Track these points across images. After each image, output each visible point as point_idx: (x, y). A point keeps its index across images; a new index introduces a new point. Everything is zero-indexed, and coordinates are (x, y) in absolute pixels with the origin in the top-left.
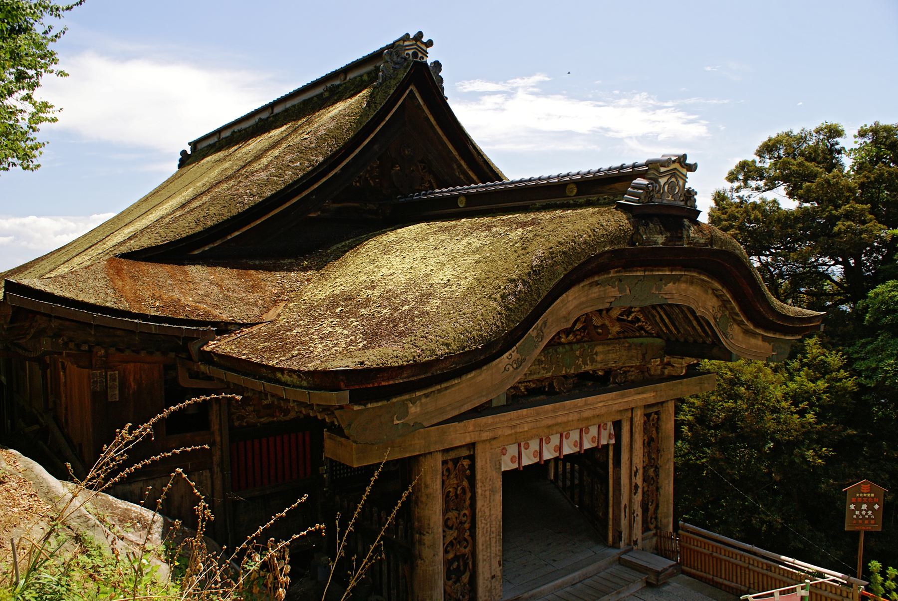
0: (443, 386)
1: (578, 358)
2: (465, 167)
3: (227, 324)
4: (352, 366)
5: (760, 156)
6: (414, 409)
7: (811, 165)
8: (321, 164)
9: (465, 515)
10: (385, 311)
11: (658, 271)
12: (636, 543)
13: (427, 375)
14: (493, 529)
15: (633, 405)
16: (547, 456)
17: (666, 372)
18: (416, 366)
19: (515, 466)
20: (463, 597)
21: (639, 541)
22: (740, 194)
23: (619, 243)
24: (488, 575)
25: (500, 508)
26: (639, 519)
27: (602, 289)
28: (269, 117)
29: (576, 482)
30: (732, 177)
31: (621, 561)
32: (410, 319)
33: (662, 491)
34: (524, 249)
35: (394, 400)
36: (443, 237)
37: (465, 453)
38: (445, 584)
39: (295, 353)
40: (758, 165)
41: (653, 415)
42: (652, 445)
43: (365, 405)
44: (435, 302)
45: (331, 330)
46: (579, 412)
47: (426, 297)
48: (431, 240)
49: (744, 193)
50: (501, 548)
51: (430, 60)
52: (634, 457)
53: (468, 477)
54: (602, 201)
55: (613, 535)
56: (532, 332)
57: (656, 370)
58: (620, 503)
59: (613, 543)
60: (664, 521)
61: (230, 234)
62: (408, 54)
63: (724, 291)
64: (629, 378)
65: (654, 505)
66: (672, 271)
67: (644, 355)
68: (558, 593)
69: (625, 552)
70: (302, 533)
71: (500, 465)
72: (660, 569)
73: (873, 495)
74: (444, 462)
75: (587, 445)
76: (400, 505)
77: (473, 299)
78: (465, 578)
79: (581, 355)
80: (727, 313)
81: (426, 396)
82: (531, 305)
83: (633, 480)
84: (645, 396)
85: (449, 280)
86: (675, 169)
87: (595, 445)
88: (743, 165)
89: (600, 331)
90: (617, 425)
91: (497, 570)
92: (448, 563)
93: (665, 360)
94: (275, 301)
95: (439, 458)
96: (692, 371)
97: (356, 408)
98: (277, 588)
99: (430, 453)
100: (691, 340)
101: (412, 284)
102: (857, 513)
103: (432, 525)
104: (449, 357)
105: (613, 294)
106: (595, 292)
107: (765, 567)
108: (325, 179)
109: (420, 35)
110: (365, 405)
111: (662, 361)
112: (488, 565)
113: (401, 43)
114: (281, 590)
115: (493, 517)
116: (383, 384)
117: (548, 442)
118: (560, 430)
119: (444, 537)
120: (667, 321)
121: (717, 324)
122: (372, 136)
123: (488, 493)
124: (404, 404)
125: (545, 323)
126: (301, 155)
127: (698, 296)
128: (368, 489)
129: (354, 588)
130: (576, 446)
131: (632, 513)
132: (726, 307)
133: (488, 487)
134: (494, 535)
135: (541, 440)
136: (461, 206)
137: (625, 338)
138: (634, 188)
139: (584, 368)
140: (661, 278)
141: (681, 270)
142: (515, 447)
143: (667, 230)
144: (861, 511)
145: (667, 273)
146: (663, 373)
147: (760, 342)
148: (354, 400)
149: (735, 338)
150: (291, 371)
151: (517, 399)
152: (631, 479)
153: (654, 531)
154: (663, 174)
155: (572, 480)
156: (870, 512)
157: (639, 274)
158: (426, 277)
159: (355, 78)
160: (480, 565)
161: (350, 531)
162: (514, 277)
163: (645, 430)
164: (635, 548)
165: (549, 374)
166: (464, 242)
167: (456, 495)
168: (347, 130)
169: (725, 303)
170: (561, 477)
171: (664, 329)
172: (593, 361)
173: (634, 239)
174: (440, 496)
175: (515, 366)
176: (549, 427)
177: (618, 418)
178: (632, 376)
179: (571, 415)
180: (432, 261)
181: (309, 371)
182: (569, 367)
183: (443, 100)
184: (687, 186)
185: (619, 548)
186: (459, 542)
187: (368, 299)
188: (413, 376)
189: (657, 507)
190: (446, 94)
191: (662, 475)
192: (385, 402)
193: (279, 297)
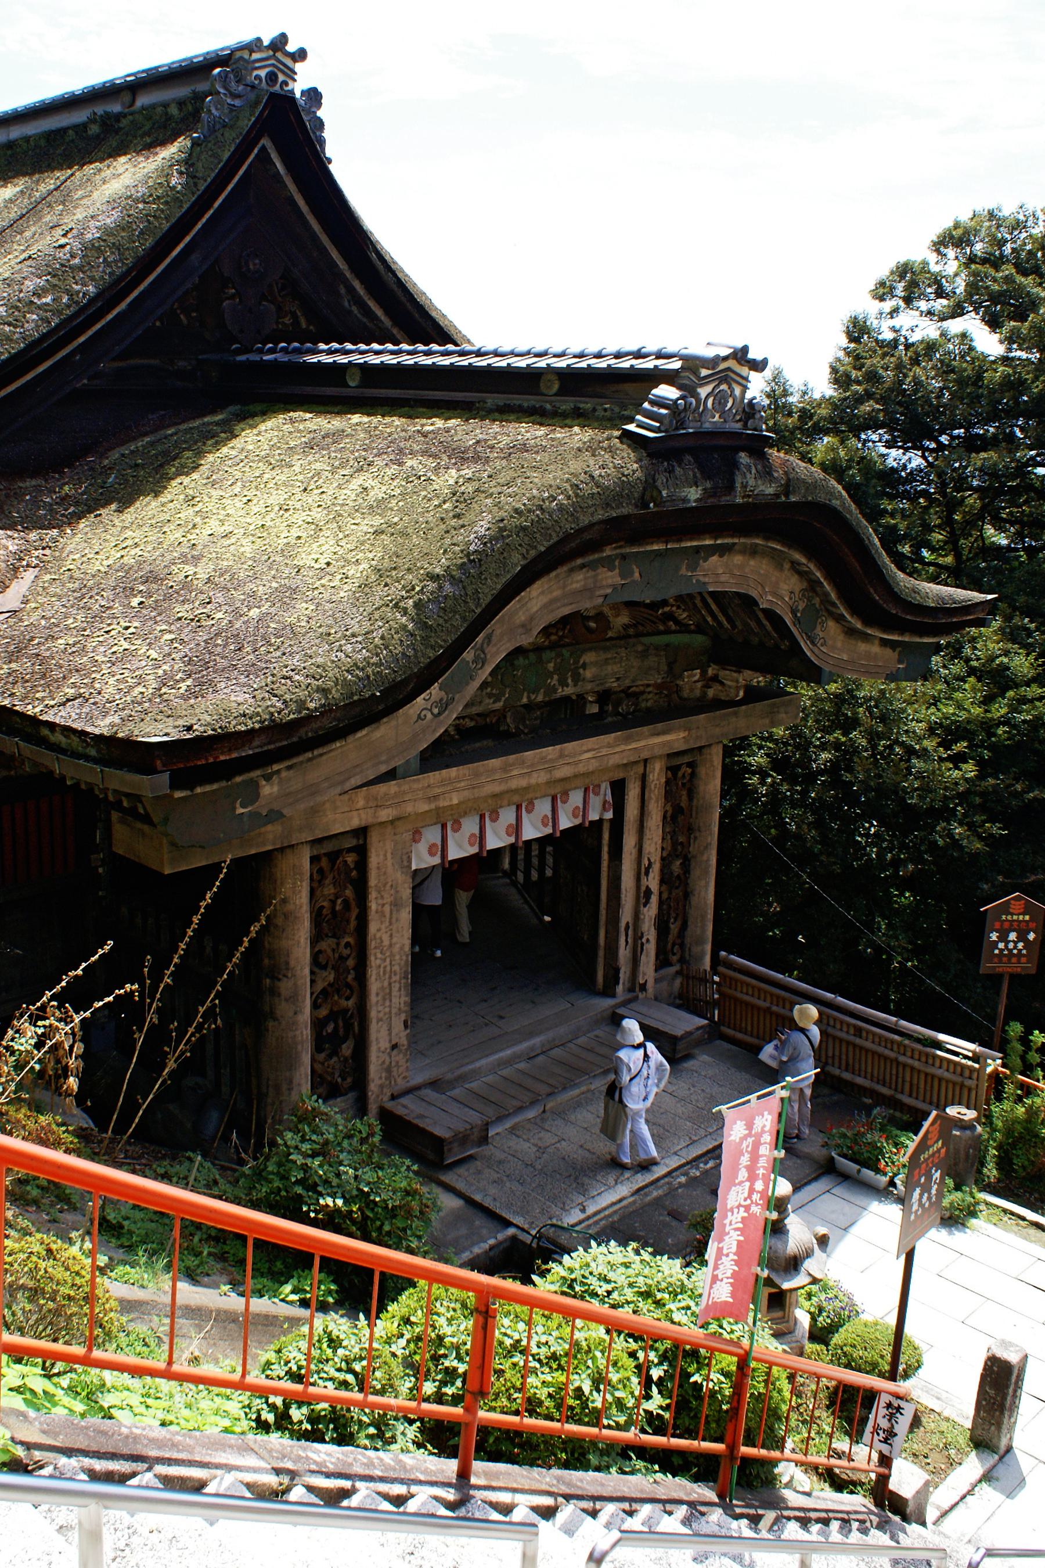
0: (316, 752)
1: (550, 675)
2: (361, 291)
4: (175, 735)
5: (938, 251)
6: (268, 790)
7: (1028, 282)
8: (92, 301)
10: (220, 615)
11: (691, 540)
12: (643, 987)
14: (396, 968)
15: (645, 755)
16: (493, 843)
17: (711, 693)
18: (274, 728)
20: (344, 1079)
22: (896, 322)
23: (620, 505)
24: (385, 1044)
25: (408, 933)
26: (651, 948)
27: (591, 573)
29: (549, 873)
30: (882, 291)
32: (264, 638)
33: (694, 900)
34: (457, 516)
35: (238, 779)
36: (318, 466)
37: (352, 842)
38: (313, 1060)
39: (71, 692)
40: (934, 268)
41: (684, 769)
42: (680, 820)
43: (192, 789)
44: (304, 608)
45: (126, 645)
46: (549, 770)
47: (286, 595)
48: (297, 469)
49: (906, 319)
50: (408, 999)
51: (298, 88)
54: (600, 413)
55: (605, 976)
56: (468, 655)
57: (692, 690)
60: (696, 950)
62: (258, 77)
63: (812, 566)
64: (643, 705)
65: (679, 923)
67: (670, 665)
68: (505, 1072)
70: (107, 1000)
71: (410, 861)
72: (679, 1033)
73: (1027, 918)
74: (314, 859)
75: (565, 823)
76: (246, 944)
77: (369, 609)
78: (347, 1049)
79: (557, 670)
80: (817, 601)
81: (289, 768)
82: (464, 619)
83: (644, 881)
85: (328, 564)
86: (728, 369)
88: (903, 270)
89: (593, 625)
90: (618, 788)
91: (401, 1035)
92: (318, 1025)
93: (710, 672)
94: (16, 569)
97: (178, 794)
98: (66, 1077)
100: (755, 640)
101: (266, 559)
102: (1001, 945)
103: (292, 963)
104: (326, 710)
105: (610, 581)
106: (578, 580)
107: (852, 1031)
108: (98, 326)
109: (283, 38)
110: (192, 789)
111: (704, 673)
112: (385, 1027)
113: (245, 55)
114: (71, 1079)
115: (396, 949)
116: (222, 758)
117: (495, 818)
118: (516, 798)
119: (312, 981)
120: (714, 607)
121: (797, 621)
122: (188, 239)
123: (387, 908)
124: (254, 785)
125: (489, 638)
126: (55, 281)
127: (765, 578)
128: (196, 919)
129: (171, 1074)
130: (545, 825)
131: (638, 936)
132: (815, 592)
133: (388, 899)
134: (397, 977)
135: (482, 817)
136: (352, 384)
137: (638, 635)
138: (653, 403)
139: (561, 692)
140: (697, 550)
141: (732, 537)
142: (438, 829)
143: (706, 476)
144: (1007, 942)
145: (707, 542)
146: (705, 694)
147: (876, 649)
148: (174, 785)
149: (830, 643)
150: (67, 730)
151: (438, 755)
152: (638, 879)
153: (677, 968)
154: (704, 381)
155: (541, 871)
156: (1020, 945)
157: (655, 547)
158: (288, 551)
159: (153, 107)
160: (373, 1027)
161: (168, 984)
162: (438, 570)
163: (669, 794)
164: (641, 996)
165: (499, 705)
166: (356, 483)
167: (333, 911)
168: (142, 233)
169: (813, 585)
170: (521, 865)
171: (709, 619)
172: (577, 678)
173: (647, 497)
174: (307, 916)
175: (436, 711)
176: (495, 796)
177: (619, 775)
178: (649, 701)
179: (535, 775)
180: (300, 517)
181: (101, 736)
182: (535, 691)
184: (749, 395)
185: (613, 995)
186: (338, 991)
187: (187, 584)
188: (269, 743)
190: (329, 152)
191: (695, 873)
192: (224, 784)
193: (21, 559)
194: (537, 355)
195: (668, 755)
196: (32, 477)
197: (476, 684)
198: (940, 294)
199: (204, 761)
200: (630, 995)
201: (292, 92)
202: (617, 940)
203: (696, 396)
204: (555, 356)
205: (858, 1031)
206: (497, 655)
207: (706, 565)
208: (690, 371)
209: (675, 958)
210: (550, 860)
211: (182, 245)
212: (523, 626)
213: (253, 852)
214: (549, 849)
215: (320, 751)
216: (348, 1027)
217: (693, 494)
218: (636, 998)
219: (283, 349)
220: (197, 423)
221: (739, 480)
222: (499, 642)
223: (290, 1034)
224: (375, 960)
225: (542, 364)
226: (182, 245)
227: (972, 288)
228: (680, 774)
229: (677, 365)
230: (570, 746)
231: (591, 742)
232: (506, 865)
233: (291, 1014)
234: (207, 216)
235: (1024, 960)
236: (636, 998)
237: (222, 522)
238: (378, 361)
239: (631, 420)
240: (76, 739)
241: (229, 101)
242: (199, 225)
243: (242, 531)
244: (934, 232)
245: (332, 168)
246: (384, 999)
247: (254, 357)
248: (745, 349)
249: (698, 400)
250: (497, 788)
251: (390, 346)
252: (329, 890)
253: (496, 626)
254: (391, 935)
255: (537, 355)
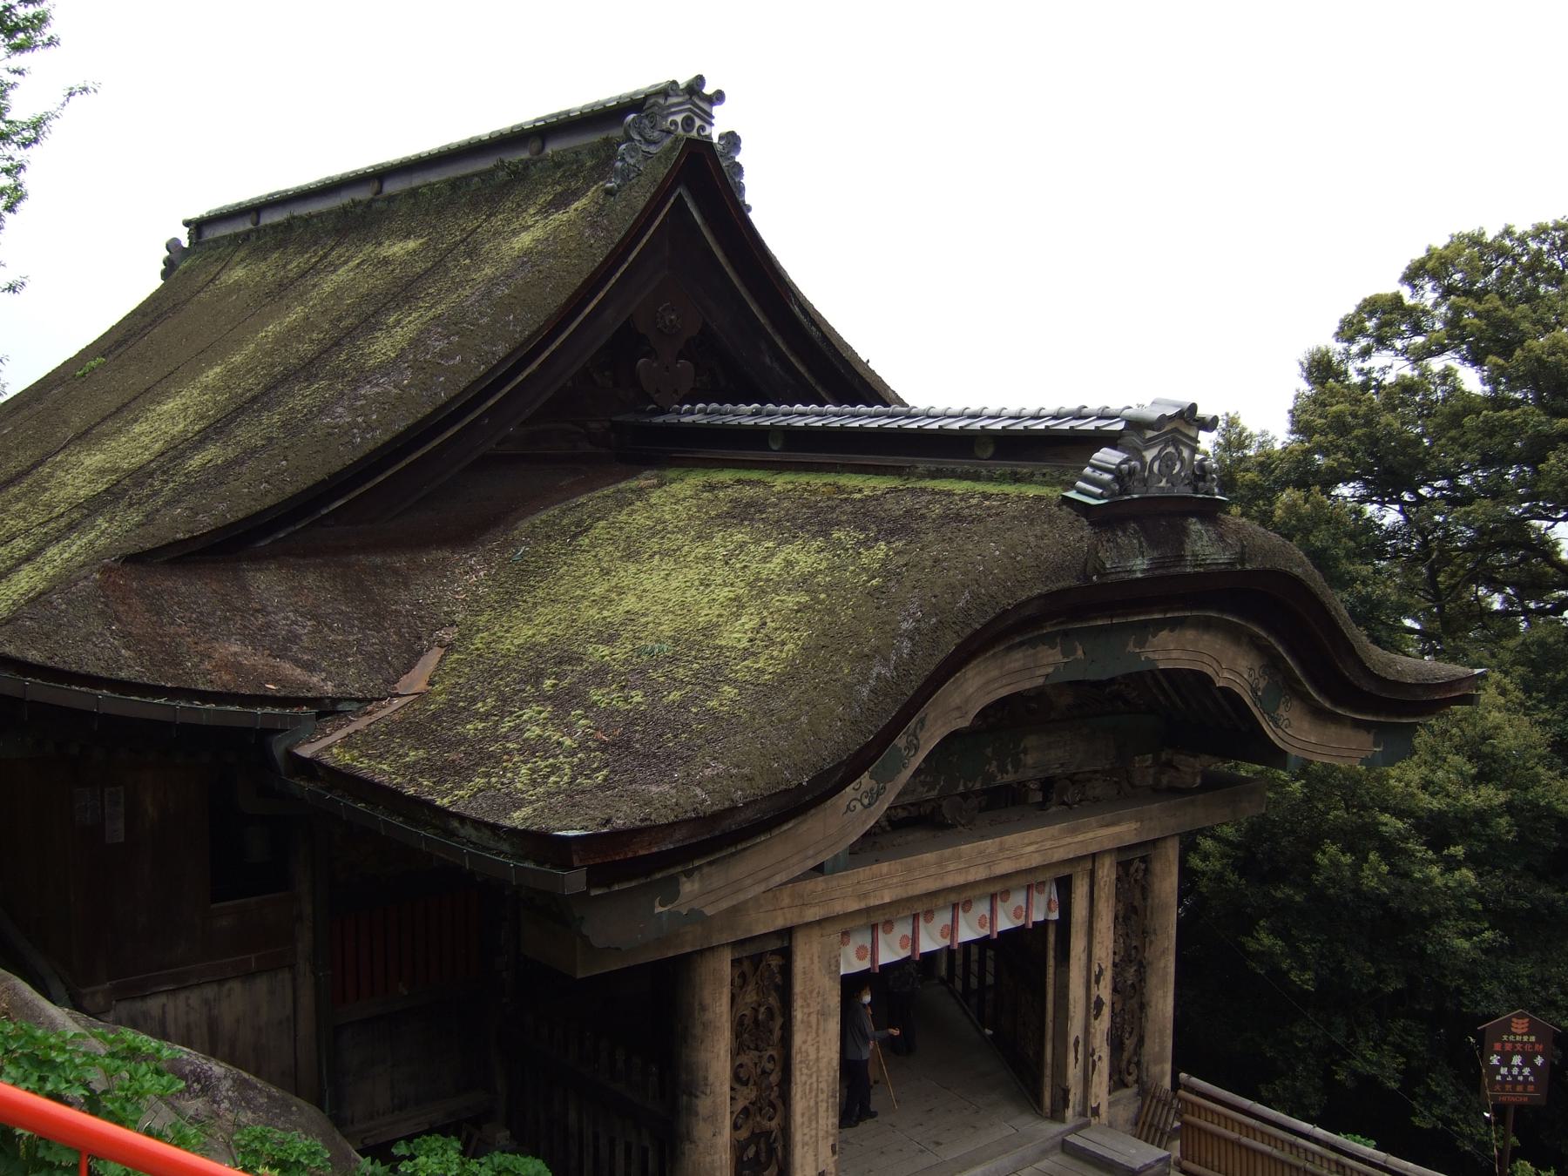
3: (336, 701)
9: (771, 1058)
11: (1139, 614)
12: (1096, 1112)
13: (717, 836)
19: (865, 965)
21: (1103, 1109)
26: (1104, 1067)
27: (1031, 651)
28: (372, 200)
29: (990, 980)
30: (1349, 330)
31: (1067, 1148)
33: (1151, 1012)
36: (739, 537)
37: (775, 944)
41: (1136, 864)
47: (713, 677)
49: (1379, 360)
51: (715, 133)
52: (1093, 950)
53: (777, 988)
56: (901, 741)
58: (1065, 1034)
59: (1053, 1111)
61: (326, 505)
62: (674, 123)
65: (1135, 1039)
66: (1166, 612)
69: (1076, 1130)
71: (838, 966)
72: (1137, 1165)
81: (710, 864)
83: (1095, 991)
84: (1117, 829)
87: (1020, 923)
88: (1371, 306)
90: (1065, 886)
92: (738, 1148)
93: (1164, 757)
95: (726, 958)
96: (1213, 784)
97: (594, 892)
99: (712, 949)
102: (1504, 1071)
103: (711, 1078)
105: (1051, 660)
106: (1017, 660)
109: (700, 80)
110: (609, 886)
115: (823, 1063)
116: (642, 852)
119: (732, 1098)
121: (1258, 700)
122: (601, 294)
123: (813, 1019)
125: (922, 721)
130: (982, 926)
131: (1089, 1053)
133: (815, 1007)
136: (775, 447)
138: (1096, 467)
140: (1145, 624)
141: (1183, 609)
144: (1510, 1067)
148: (591, 883)
151: (870, 846)
156: (1526, 1071)
157: (1100, 623)
164: (1094, 1121)
165: (933, 794)
167: (756, 1020)
170: (959, 971)
172: (1017, 765)
175: (866, 801)
177: (1065, 871)
183: (741, 211)
185: (1063, 1120)
189: (1141, 1041)
190: (748, 199)
191: (1153, 981)
194: (970, 417)
195: (1119, 849)
196: (439, 547)
197: (907, 773)
198: (1417, 329)
199: (632, 860)
200: (1082, 1120)
201: (709, 136)
202: (1066, 1057)
203: (1142, 460)
204: (990, 417)
205: (1292, 1145)
206: (931, 739)
207: (1155, 641)
208: (1135, 430)
209: (1131, 1079)
210: (990, 965)
211: (595, 301)
212: (958, 708)
213: (671, 954)
214: (990, 953)
215: (744, 845)
216: (771, 1151)
217: (1140, 565)
218: (1088, 1124)
219: (700, 411)
220: (612, 489)
221: (1188, 549)
222: (934, 728)
223: (708, 1159)
224: (800, 1077)
225: (977, 425)
226: (595, 301)
227: (1453, 323)
228: (1132, 870)
229: (1120, 426)
230: (1010, 840)
231: (1034, 834)
232: (943, 972)
233: (709, 1134)
234: (622, 270)
235: (1531, 1088)
236: (1088, 1124)
237: (640, 598)
238: (802, 424)
239: (1072, 486)
240: (488, 833)
241: (644, 148)
242: (613, 281)
243: (660, 608)
244: (1401, 268)
245: (752, 216)
246: (810, 1121)
247: (671, 419)
248: (1193, 407)
249: (1143, 463)
250: (932, 885)
251: (814, 407)
252: (751, 997)
253: (930, 710)
254: (817, 1047)
255: (970, 417)
